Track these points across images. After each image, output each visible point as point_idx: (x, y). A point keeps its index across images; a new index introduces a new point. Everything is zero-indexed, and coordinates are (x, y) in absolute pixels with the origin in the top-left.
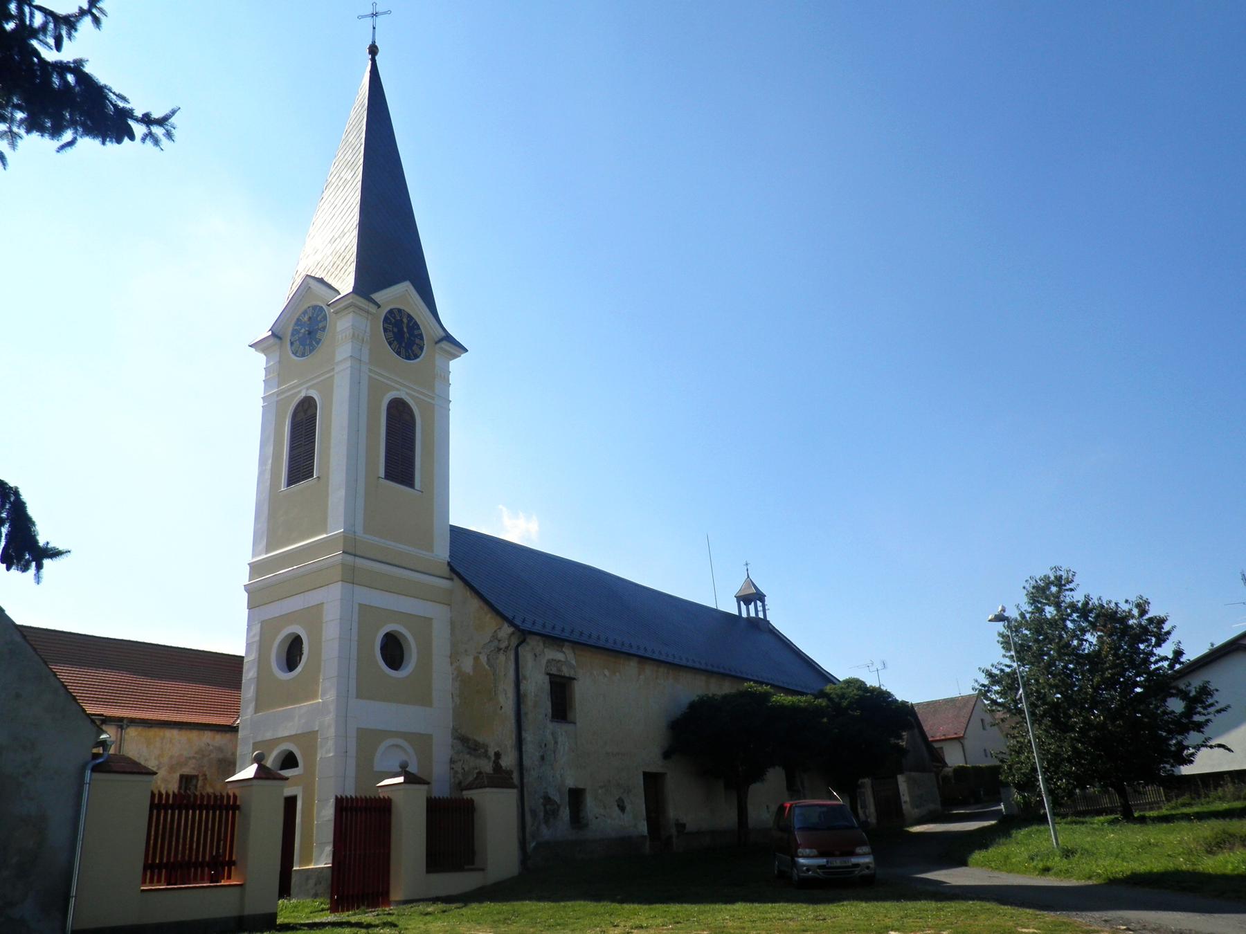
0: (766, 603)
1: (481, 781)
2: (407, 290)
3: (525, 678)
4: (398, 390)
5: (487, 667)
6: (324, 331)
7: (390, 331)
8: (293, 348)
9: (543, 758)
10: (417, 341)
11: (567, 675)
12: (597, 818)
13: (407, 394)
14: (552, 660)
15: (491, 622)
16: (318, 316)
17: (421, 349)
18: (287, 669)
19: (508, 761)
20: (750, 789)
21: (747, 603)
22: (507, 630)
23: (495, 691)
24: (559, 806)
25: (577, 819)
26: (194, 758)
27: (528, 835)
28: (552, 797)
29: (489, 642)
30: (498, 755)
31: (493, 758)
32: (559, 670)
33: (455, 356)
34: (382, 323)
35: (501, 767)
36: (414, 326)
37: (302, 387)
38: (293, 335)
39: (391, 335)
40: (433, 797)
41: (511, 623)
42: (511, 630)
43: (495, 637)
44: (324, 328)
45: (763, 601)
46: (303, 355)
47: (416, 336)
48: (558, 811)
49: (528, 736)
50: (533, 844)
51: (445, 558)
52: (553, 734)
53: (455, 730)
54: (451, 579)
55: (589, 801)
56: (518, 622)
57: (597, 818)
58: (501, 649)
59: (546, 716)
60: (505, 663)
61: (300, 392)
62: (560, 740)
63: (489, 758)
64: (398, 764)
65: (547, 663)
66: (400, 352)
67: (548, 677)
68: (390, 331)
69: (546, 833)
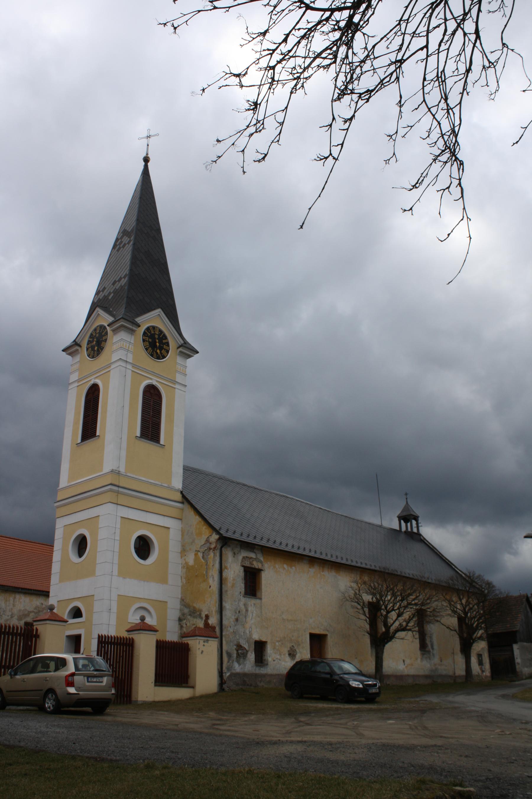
0: (419, 522)
1: (195, 633)
2: (159, 314)
3: (226, 568)
4: (151, 379)
5: (202, 560)
6: (106, 342)
7: (147, 341)
8: (158, 329)
9: (237, 620)
10: (165, 347)
11: (257, 567)
12: (274, 661)
13: (157, 381)
14: (247, 557)
15: (206, 531)
16: (103, 332)
17: (168, 352)
18: (78, 557)
19: (213, 621)
20: (385, 648)
21: (406, 521)
22: (215, 537)
23: (207, 576)
24: (247, 651)
25: (260, 660)
26: (33, 612)
27: (224, 668)
28: (243, 645)
29: (204, 544)
30: (207, 617)
31: (204, 619)
32: (251, 563)
33: (190, 356)
34: (142, 336)
35: (209, 624)
36: (163, 337)
37: (92, 378)
38: (88, 344)
39: (148, 343)
40: (167, 641)
41: (218, 532)
42: (217, 537)
43: (207, 541)
44: (106, 340)
45: (417, 520)
46: (93, 357)
47: (164, 344)
48: (247, 654)
49: (227, 605)
50: (228, 674)
51: (180, 489)
52: (245, 605)
53: (182, 600)
54: (182, 503)
55: (269, 650)
56: (222, 532)
57: (274, 661)
58: (211, 549)
59: (240, 593)
60: (213, 559)
61: (91, 380)
62: (250, 609)
63: (202, 618)
64: (139, 618)
65: (242, 559)
66: (153, 354)
67: (242, 568)
68: (147, 341)
69: (237, 668)
